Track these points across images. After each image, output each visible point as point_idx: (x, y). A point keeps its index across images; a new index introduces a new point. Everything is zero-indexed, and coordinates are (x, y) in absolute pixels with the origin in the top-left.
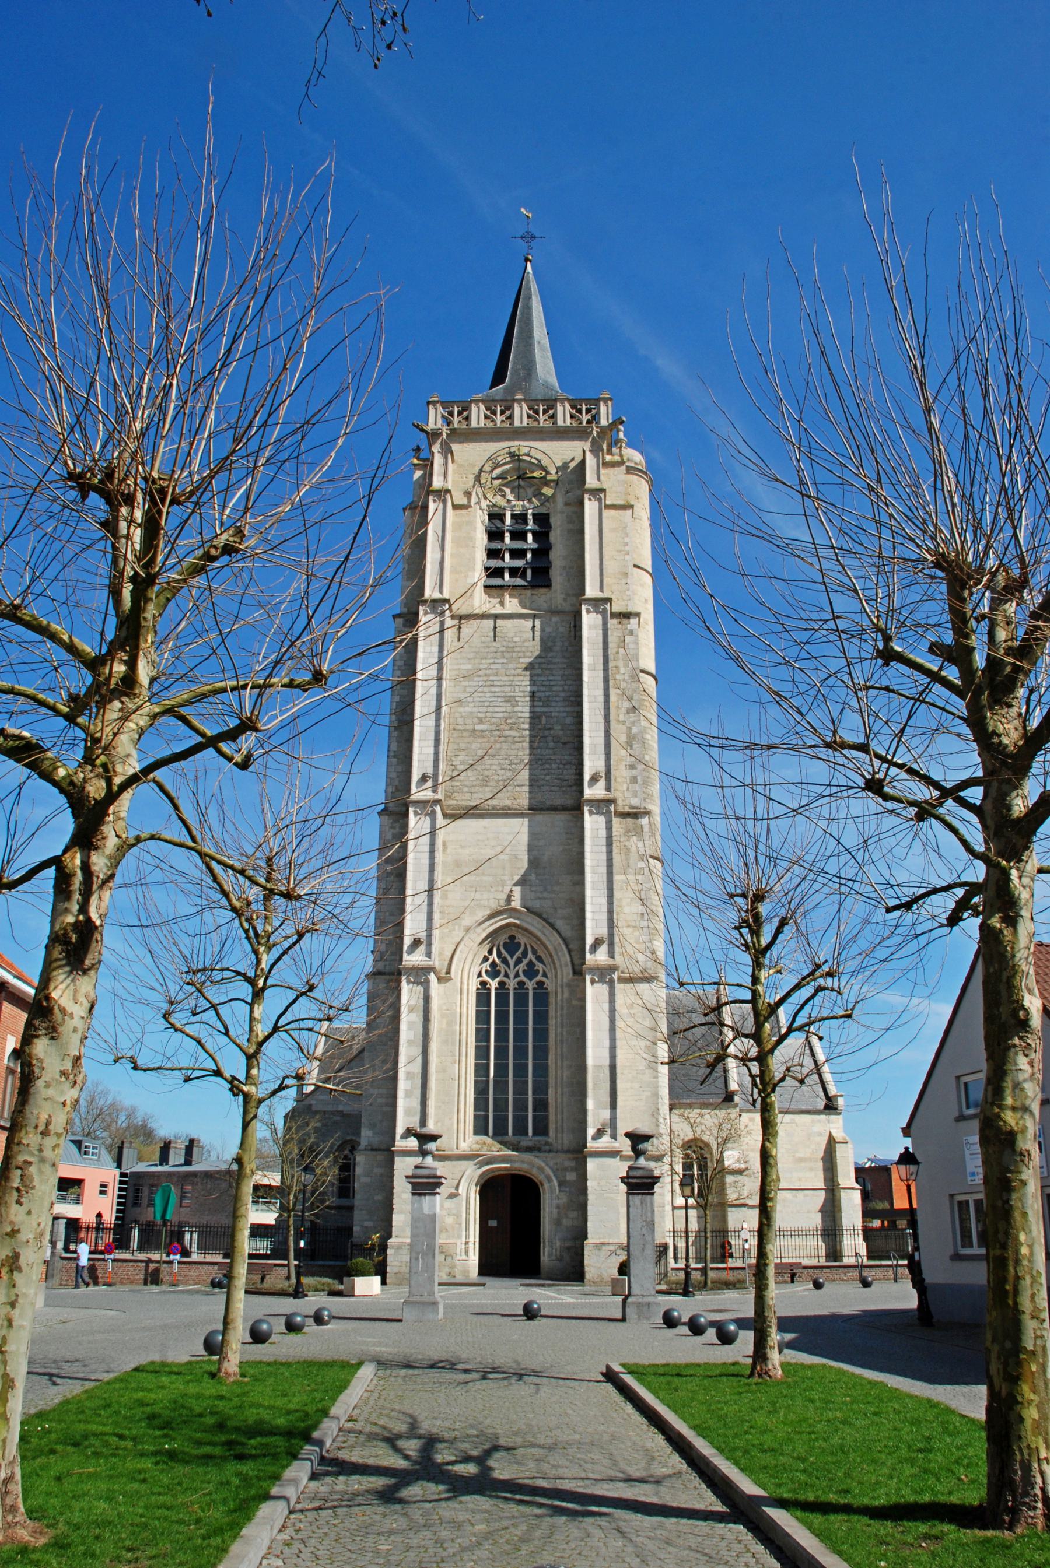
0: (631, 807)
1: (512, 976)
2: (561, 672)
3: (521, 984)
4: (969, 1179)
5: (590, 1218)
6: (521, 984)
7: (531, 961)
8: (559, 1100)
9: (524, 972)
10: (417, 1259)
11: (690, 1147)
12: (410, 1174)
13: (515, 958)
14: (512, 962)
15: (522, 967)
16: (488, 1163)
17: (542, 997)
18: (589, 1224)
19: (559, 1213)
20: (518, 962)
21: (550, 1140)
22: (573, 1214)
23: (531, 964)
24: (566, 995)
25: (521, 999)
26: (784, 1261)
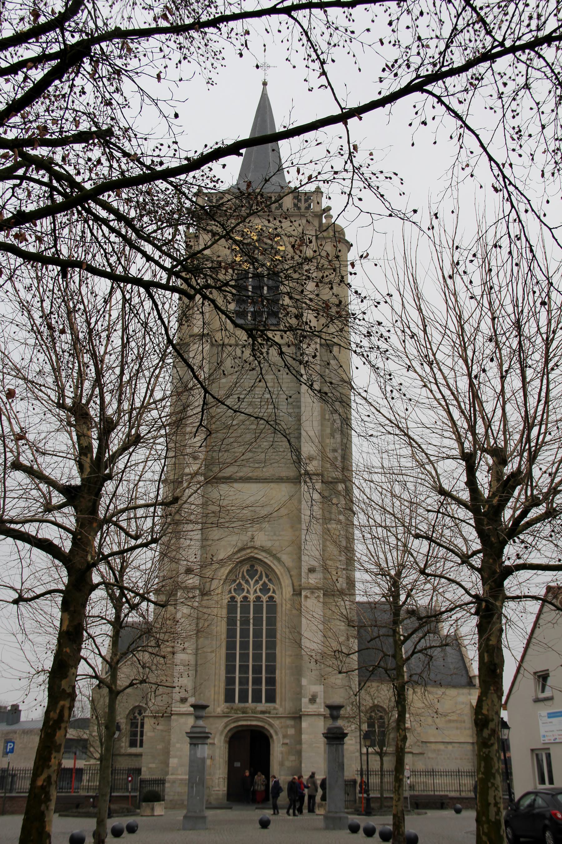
0: (333, 478)
1: (252, 592)
2: (287, 385)
3: (258, 598)
4: (542, 739)
5: (303, 761)
6: (258, 598)
7: (265, 582)
8: (283, 678)
9: (260, 589)
10: (192, 787)
11: (374, 711)
12: (189, 731)
13: (254, 580)
14: (252, 583)
15: (258, 586)
16: (234, 722)
17: (272, 606)
18: (303, 765)
19: (282, 757)
20: (257, 582)
21: (277, 706)
22: (292, 758)
23: (265, 584)
24: (289, 606)
25: (258, 609)
26: (436, 793)
